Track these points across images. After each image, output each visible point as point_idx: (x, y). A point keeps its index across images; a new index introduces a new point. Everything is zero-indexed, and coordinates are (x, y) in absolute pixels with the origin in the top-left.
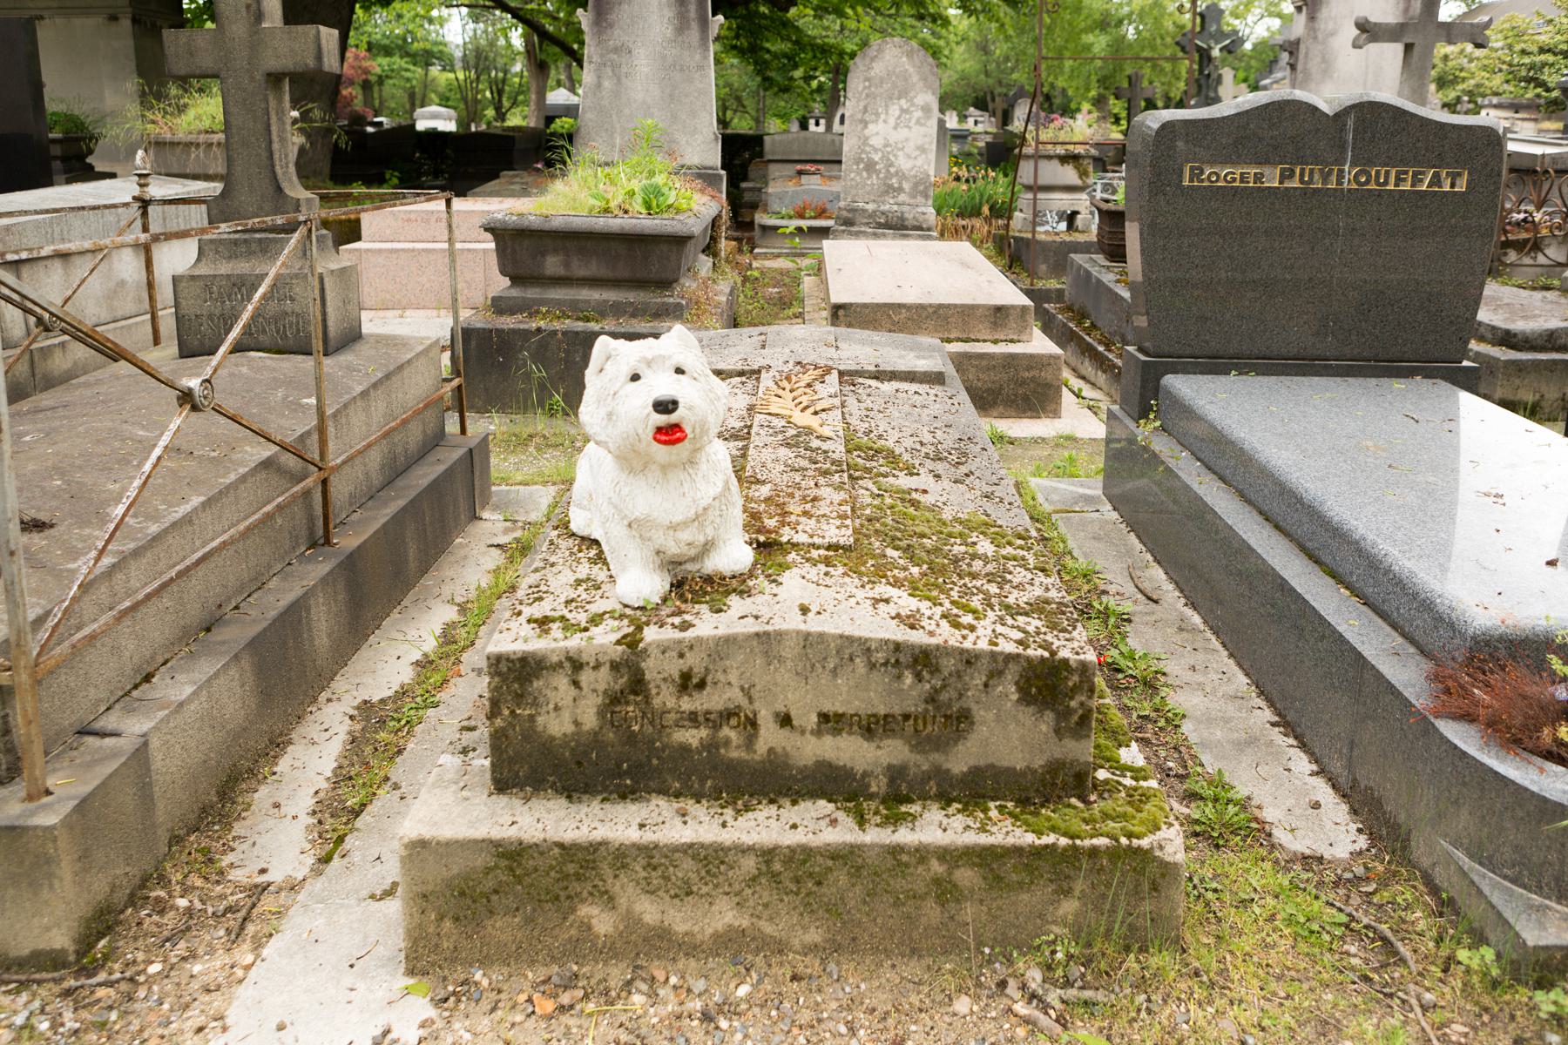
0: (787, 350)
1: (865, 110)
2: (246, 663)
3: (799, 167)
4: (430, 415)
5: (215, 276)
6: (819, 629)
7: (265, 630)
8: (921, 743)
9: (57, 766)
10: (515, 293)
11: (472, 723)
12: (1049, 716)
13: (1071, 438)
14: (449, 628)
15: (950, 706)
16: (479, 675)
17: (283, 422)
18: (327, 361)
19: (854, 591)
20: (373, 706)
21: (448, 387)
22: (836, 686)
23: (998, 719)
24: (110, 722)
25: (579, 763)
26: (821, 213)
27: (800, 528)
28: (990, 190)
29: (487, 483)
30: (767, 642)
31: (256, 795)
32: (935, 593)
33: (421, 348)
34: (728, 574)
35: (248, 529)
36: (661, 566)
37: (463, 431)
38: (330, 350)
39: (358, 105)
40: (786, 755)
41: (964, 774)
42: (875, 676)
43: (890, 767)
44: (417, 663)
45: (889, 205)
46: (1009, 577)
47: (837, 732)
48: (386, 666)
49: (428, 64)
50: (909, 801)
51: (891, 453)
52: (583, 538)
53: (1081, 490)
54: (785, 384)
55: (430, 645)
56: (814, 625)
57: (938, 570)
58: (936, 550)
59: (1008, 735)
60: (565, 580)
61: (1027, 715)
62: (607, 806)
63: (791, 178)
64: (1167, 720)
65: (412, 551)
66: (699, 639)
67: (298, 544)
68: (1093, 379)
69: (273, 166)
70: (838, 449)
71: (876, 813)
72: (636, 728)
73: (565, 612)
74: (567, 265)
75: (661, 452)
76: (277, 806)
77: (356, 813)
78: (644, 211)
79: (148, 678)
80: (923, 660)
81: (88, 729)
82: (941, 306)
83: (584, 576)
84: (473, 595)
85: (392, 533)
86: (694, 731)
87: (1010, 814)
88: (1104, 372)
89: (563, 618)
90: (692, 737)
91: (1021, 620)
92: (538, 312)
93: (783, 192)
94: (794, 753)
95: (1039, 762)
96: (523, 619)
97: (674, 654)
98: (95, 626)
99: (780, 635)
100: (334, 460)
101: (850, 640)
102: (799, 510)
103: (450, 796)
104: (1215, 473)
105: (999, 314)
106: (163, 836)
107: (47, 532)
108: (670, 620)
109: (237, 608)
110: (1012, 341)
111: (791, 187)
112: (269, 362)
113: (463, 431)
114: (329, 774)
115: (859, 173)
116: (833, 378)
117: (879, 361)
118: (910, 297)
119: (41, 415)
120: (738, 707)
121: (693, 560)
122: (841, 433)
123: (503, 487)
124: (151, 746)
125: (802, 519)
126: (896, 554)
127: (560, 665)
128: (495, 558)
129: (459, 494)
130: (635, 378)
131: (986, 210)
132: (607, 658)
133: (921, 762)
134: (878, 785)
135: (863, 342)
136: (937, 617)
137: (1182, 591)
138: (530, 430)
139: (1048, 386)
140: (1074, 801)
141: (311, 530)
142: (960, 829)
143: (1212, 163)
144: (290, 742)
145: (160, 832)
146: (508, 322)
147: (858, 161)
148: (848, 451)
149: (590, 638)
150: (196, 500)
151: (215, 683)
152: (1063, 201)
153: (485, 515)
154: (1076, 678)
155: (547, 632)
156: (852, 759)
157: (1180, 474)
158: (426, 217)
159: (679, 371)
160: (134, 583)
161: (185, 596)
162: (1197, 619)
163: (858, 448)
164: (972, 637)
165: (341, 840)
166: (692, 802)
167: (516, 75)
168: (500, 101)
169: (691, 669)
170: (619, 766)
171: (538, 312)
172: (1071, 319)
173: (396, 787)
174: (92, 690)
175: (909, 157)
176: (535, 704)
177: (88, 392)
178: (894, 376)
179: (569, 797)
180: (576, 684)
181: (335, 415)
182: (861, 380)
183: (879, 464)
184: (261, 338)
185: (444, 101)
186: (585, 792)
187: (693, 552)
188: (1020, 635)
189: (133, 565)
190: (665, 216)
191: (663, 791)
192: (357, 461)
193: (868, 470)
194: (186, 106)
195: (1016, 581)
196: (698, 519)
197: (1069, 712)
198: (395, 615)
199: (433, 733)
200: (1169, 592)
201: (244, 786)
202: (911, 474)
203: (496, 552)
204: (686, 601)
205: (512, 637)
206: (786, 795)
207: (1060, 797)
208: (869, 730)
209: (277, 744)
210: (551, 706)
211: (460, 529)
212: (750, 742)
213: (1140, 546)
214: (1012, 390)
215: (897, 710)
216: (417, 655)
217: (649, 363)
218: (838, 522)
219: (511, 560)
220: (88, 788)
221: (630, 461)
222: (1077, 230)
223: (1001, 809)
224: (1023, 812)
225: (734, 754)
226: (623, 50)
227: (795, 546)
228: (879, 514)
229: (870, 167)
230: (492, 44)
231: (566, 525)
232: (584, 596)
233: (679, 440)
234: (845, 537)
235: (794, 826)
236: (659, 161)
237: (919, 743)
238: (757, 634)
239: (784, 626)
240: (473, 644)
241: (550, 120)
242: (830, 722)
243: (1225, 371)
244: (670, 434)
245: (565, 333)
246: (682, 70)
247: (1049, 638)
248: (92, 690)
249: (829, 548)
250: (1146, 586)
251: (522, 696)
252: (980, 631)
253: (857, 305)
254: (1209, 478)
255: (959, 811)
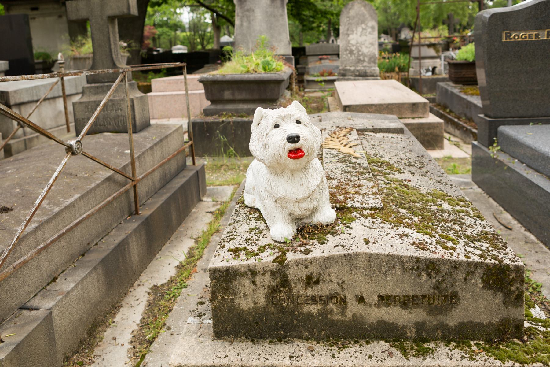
0: (331, 122)
1: (348, 30)
2: (100, 271)
3: (320, 57)
4: (180, 157)
5: (89, 102)
6: (377, 252)
7: (108, 255)
8: (432, 311)
9: (8, 326)
10: (213, 107)
11: (203, 300)
12: (500, 295)
13: (450, 158)
14: (191, 249)
15: (447, 291)
16: (205, 272)
17: (117, 161)
18: (135, 136)
19: (389, 231)
20: (158, 288)
21: (187, 145)
22: (387, 281)
23: (473, 297)
24: (35, 303)
25: (257, 323)
26: (330, 74)
27: (355, 200)
28: (398, 61)
29: (205, 186)
30: (350, 259)
31: (105, 334)
32: (429, 231)
33: (175, 129)
34: (325, 224)
35: (100, 208)
36: (292, 221)
37: (194, 163)
38: (137, 131)
39: (151, 46)
40: (362, 317)
41: (456, 326)
42: (407, 275)
43: (416, 323)
44: (177, 267)
45: (360, 67)
46: (463, 221)
47: (388, 305)
48: (164, 268)
49: (176, 30)
50: (428, 341)
51: (388, 164)
52: (251, 208)
53: (462, 180)
54: (334, 135)
55: (182, 258)
56: (374, 249)
57: (428, 221)
58: (423, 209)
59: (478, 306)
60: (244, 229)
61: (488, 295)
62: (272, 345)
63: (317, 61)
64: (533, 288)
65: (174, 216)
66: (315, 258)
67: (124, 215)
68: (453, 133)
69: (111, 55)
70: (365, 163)
71: (412, 348)
72: (285, 305)
73: (246, 245)
74: (233, 94)
75: (292, 163)
76: (115, 339)
77: (151, 342)
78: (263, 71)
79: (54, 280)
80: (432, 267)
81: (24, 307)
82: (389, 104)
83: (253, 227)
84: (201, 234)
85: (165, 208)
86: (314, 306)
87: (484, 348)
88: (459, 129)
89: (245, 249)
90: (314, 309)
91: (477, 244)
92: (222, 114)
93: (315, 68)
94: (366, 316)
95: (496, 320)
96: (225, 249)
97: (303, 266)
98: (25, 257)
99: (356, 255)
100: (139, 176)
101: (393, 257)
102: (353, 191)
103: (193, 340)
104: (532, 168)
105: (414, 107)
106: (61, 357)
107: (9, 213)
108: (299, 249)
109: (96, 244)
110: (420, 118)
111: (318, 64)
112: (112, 137)
113: (194, 163)
114: (138, 322)
115: (347, 55)
116: (354, 132)
117: (373, 124)
118: (376, 101)
119: (17, 162)
120: (337, 293)
121: (307, 217)
122: (364, 155)
123: (212, 187)
124: (54, 314)
125: (356, 196)
126: (404, 211)
127: (245, 273)
128: (209, 218)
129: (192, 192)
130: (277, 126)
131: (397, 69)
132: (269, 269)
133: (433, 320)
134: (411, 333)
135: (363, 118)
136: (434, 243)
137: (522, 224)
138: (221, 163)
139: (438, 136)
140: (515, 340)
141: (130, 208)
142: (459, 359)
143: (515, 30)
144: (121, 306)
145: (59, 355)
146: (210, 119)
147: (346, 50)
148: (369, 164)
149: (260, 259)
150: (77, 196)
151: (85, 281)
152: (429, 63)
153: (205, 199)
154: (513, 275)
155: (238, 256)
156: (397, 319)
157: (516, 170)
158: (176, 82)
159: (298, 122)
160: (47, 235)
161: (72, 240)
162: (533, 237)
163: (373, 162)
164: (455, 254)
165: (143, 357)
166: (315, 343)
167: (208, 32)
168: (203, 42)
169: (312, 274)
170: (277, 324)
171: (222, 114)
172: (441, 109)
173: (169, 328)
174: (27, 287)
175: (367, 47)
176: (234, 293)
177: (38, 152)
178: (381, 130)
179: (253, 341)
180: (254, 283)
181: (139, 157)
182: (366, 133)
183: (384, 169)
184: (109, 127)
185: (183, 43)
186: (261, 338)
187: (308, 213)
188: (479, 252)
189: (46, 227)
190: (272, 72)
191: (300, 337)
192: (149, 177)
193: (380, 172)
194: (84, 44)
195: (468, 223)
196: (310, 197)
197: (510, 293)
198: (167, 244)
199: (185, 301)
200: (514, 223)
201: (100, 329)
202: (401, 173)
203: (209, 215)
204: (305, 238)
205: (222, 260)
206: (363, 339)
207: (508, 338)
208: (405, 304)
209: (115, 307)
210: (242, 294)
211: (194, 205)
212: (343, 311)
213: (495, 204)
214: (430, 139)
215: (419, 293)
216: (177, 263)
217: (283, 119)
218: (373, 197)
219: (216, 218)
220: (21, 338)
221: (276, 168)
222: (436, 74)
223: (478, 345)
224: (490, 347)
225: (335, 317)
226: (250, 10)
227: (355, 208)
228: (390, 192)
229: (351, 52)
230: (199, 21)
231: (243, 202)
232: (254, 237)
233: (301, 156)
234: (378, 203)
235: (370, 357)
236: (267, 52)
237: (431, 310)
238: (345, 255)
239: (359, 251)
240: (201, 257)
241: (222, 47)
242: (384, 300)
243: (528, 124)
244: (296, 154)
245: (234, 122)
246: (274, 17)
247: (495, 253)
248: (27, 287)
249: (371, 209)
250: (503, 222)
251: (227, 289)
252: (459, 251)
253: (354, 105)
254: (531, 171)
255: (456, 347)
